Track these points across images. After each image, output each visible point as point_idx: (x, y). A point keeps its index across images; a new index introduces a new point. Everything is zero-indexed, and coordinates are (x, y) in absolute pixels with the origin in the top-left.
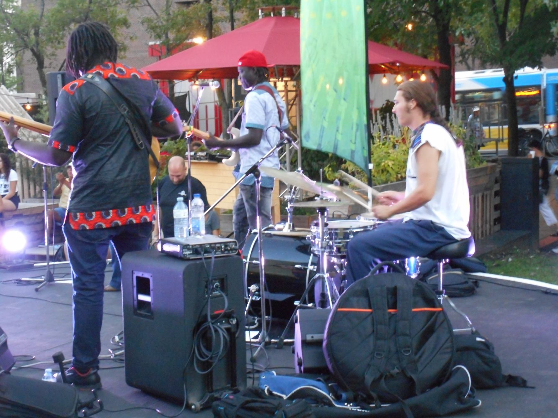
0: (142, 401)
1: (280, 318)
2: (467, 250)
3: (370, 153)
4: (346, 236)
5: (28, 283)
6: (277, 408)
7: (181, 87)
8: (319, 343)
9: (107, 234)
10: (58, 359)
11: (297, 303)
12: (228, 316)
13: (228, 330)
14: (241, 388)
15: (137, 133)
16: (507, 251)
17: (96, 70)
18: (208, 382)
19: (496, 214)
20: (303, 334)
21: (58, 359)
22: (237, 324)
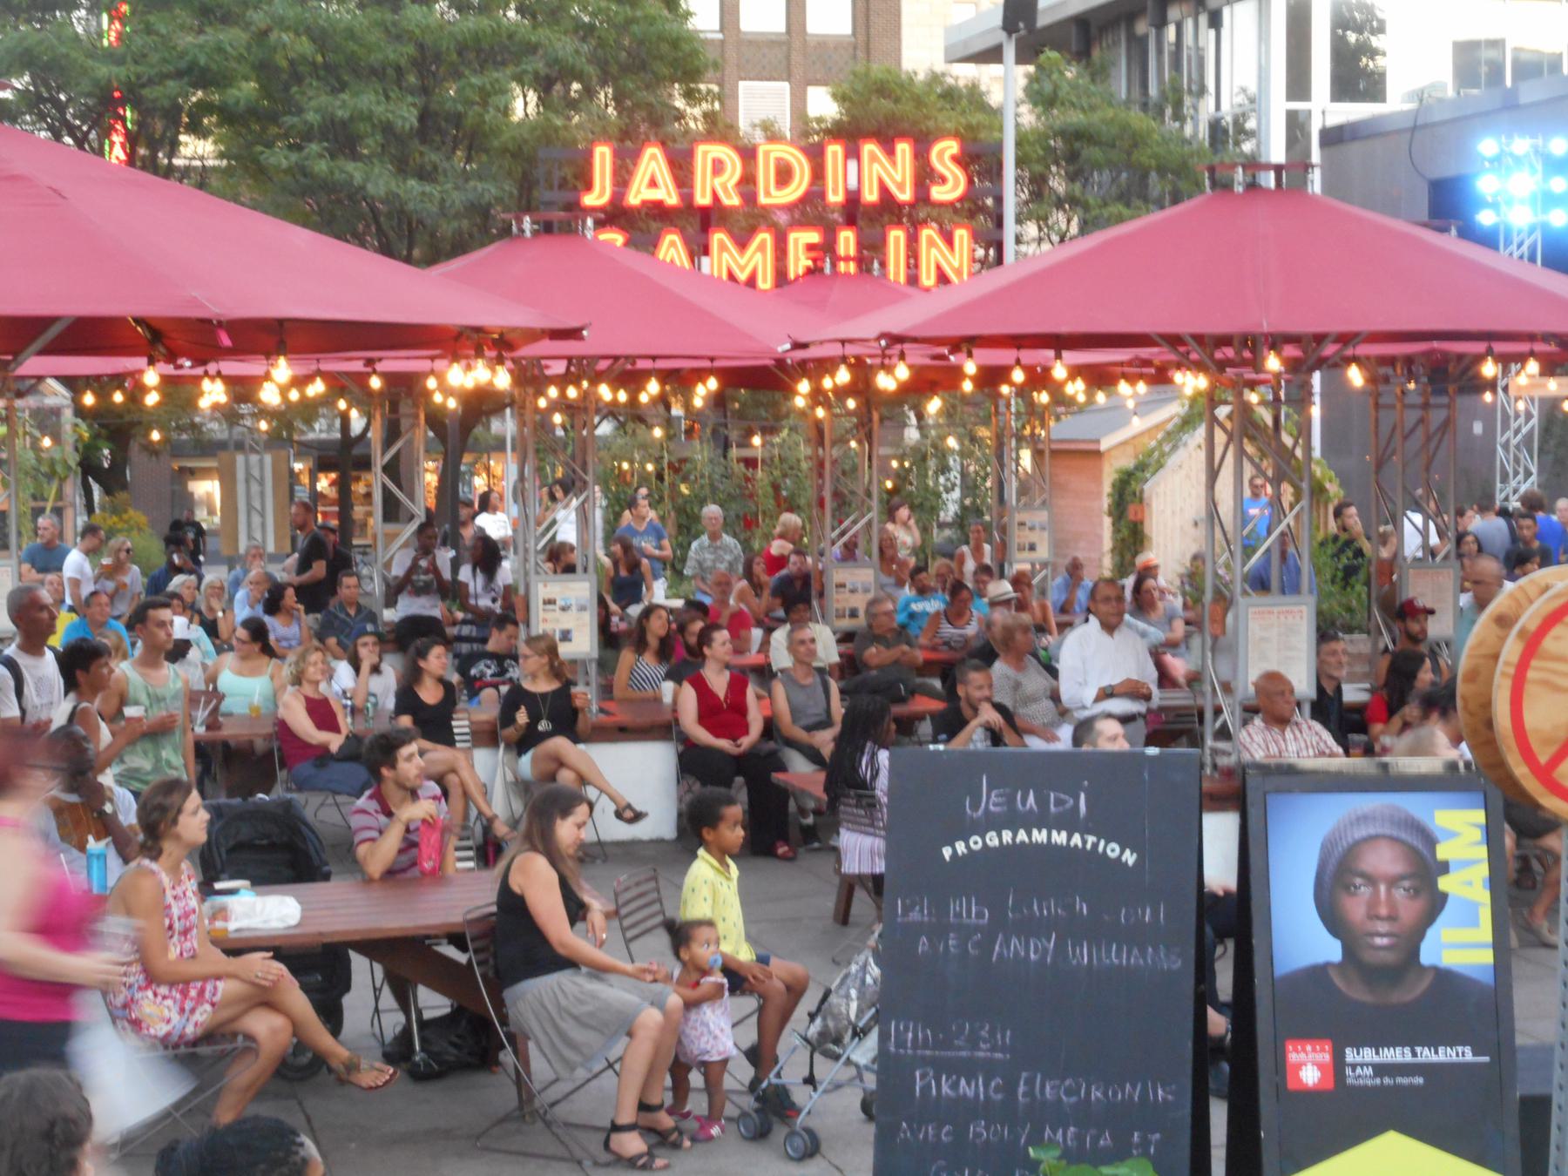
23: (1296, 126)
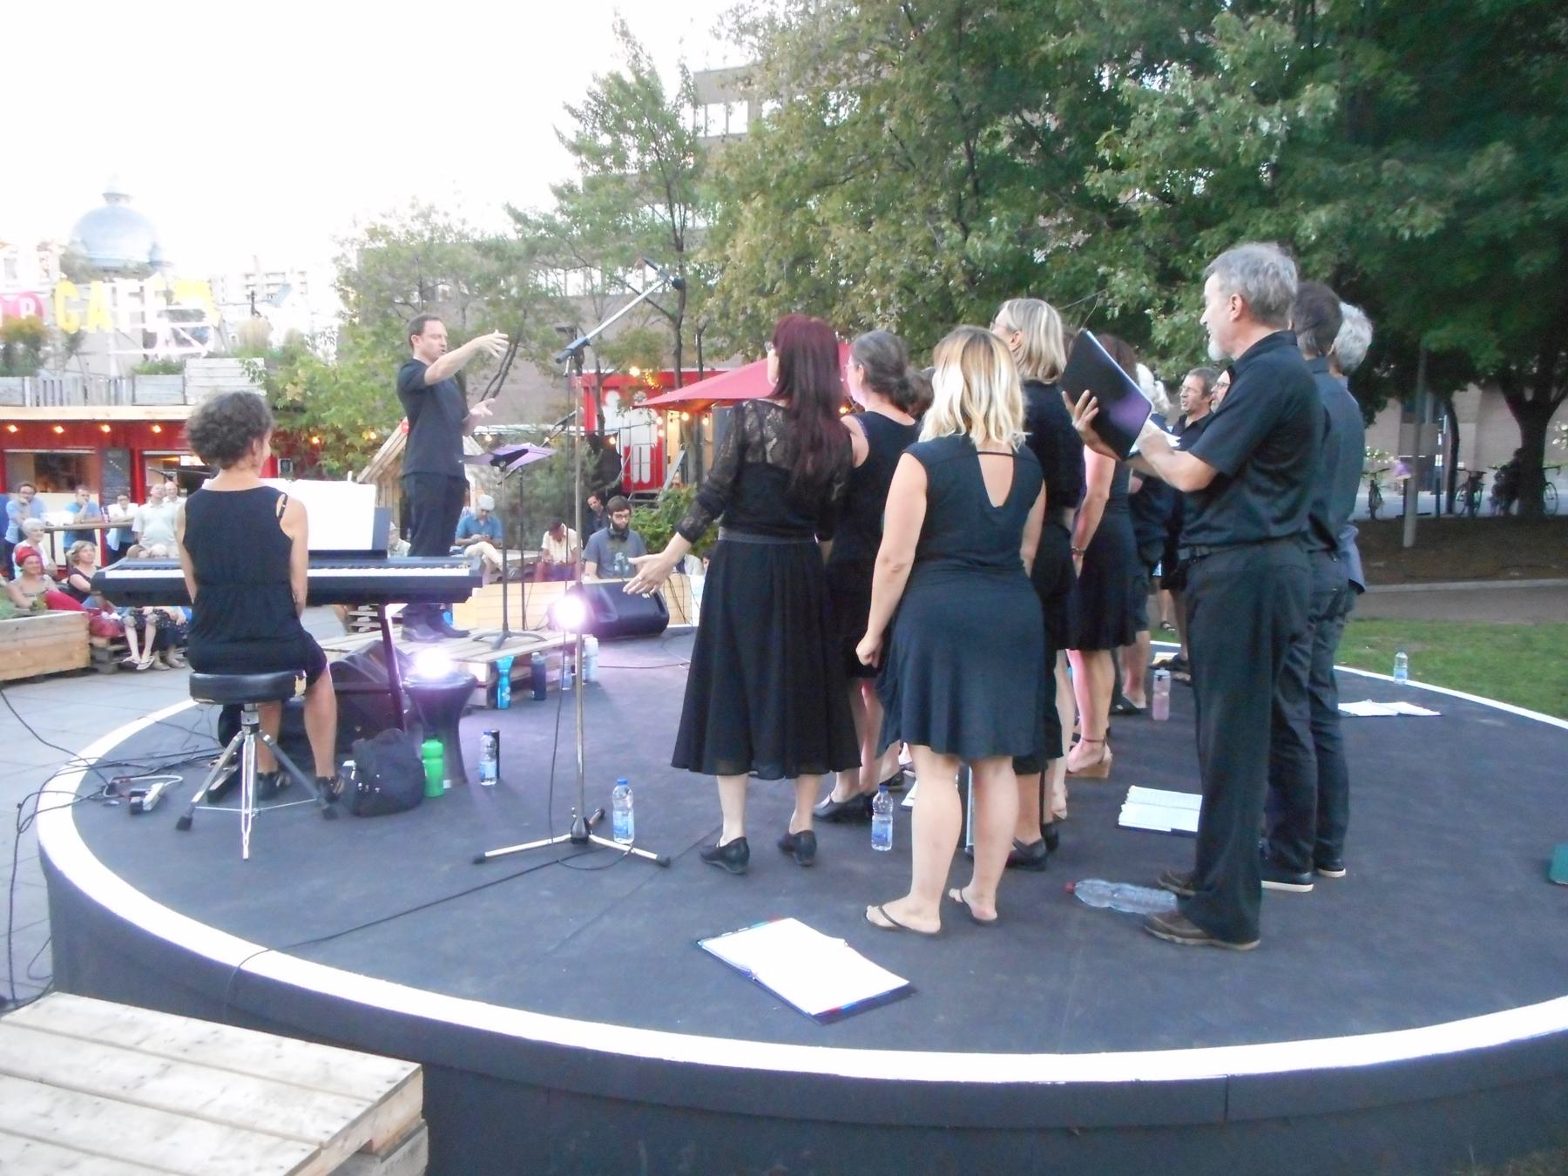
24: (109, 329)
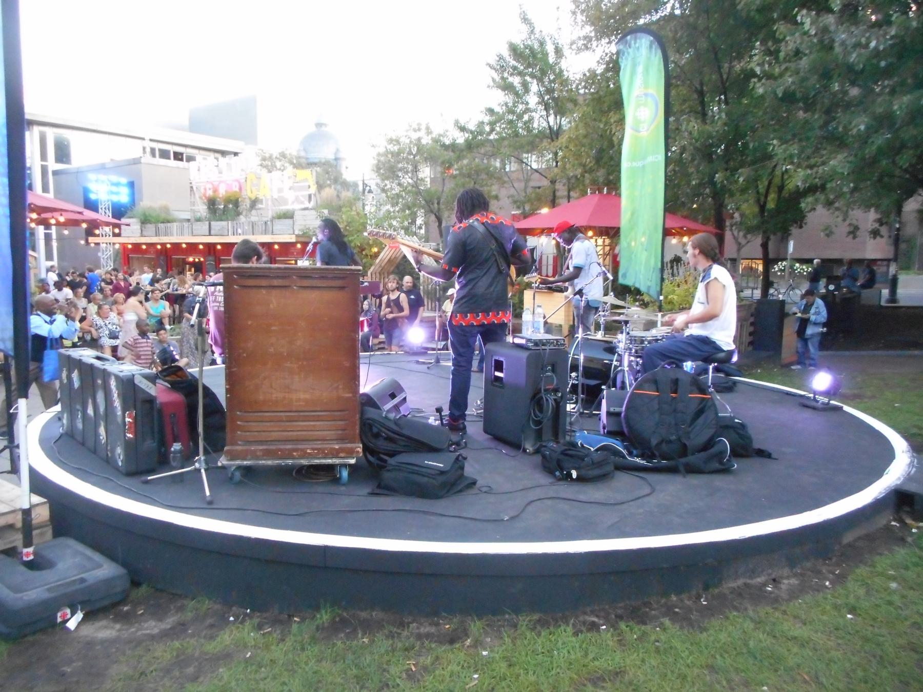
0: (493, 444)
1: (592, 397)
2: (731, 358)
3: (661, 289)
4: (642, 342)
5: (424, 363)
6: (586, 456)
7: (531, 241)
8: (618, 414)
9: (477, 329)
10: (439, 410)
11: (603, 387)
12: (556, 391)
13: (555, 400)
14: (562, 441)
15: (501, 261)
16: (758, 365)
17: (475, 217)
18: (539, 435)
19: (750, 339)
20: (608, 406)
21: (439, 410)
22: (562, 397)
23: (44, 170)
24: (269, 197)
